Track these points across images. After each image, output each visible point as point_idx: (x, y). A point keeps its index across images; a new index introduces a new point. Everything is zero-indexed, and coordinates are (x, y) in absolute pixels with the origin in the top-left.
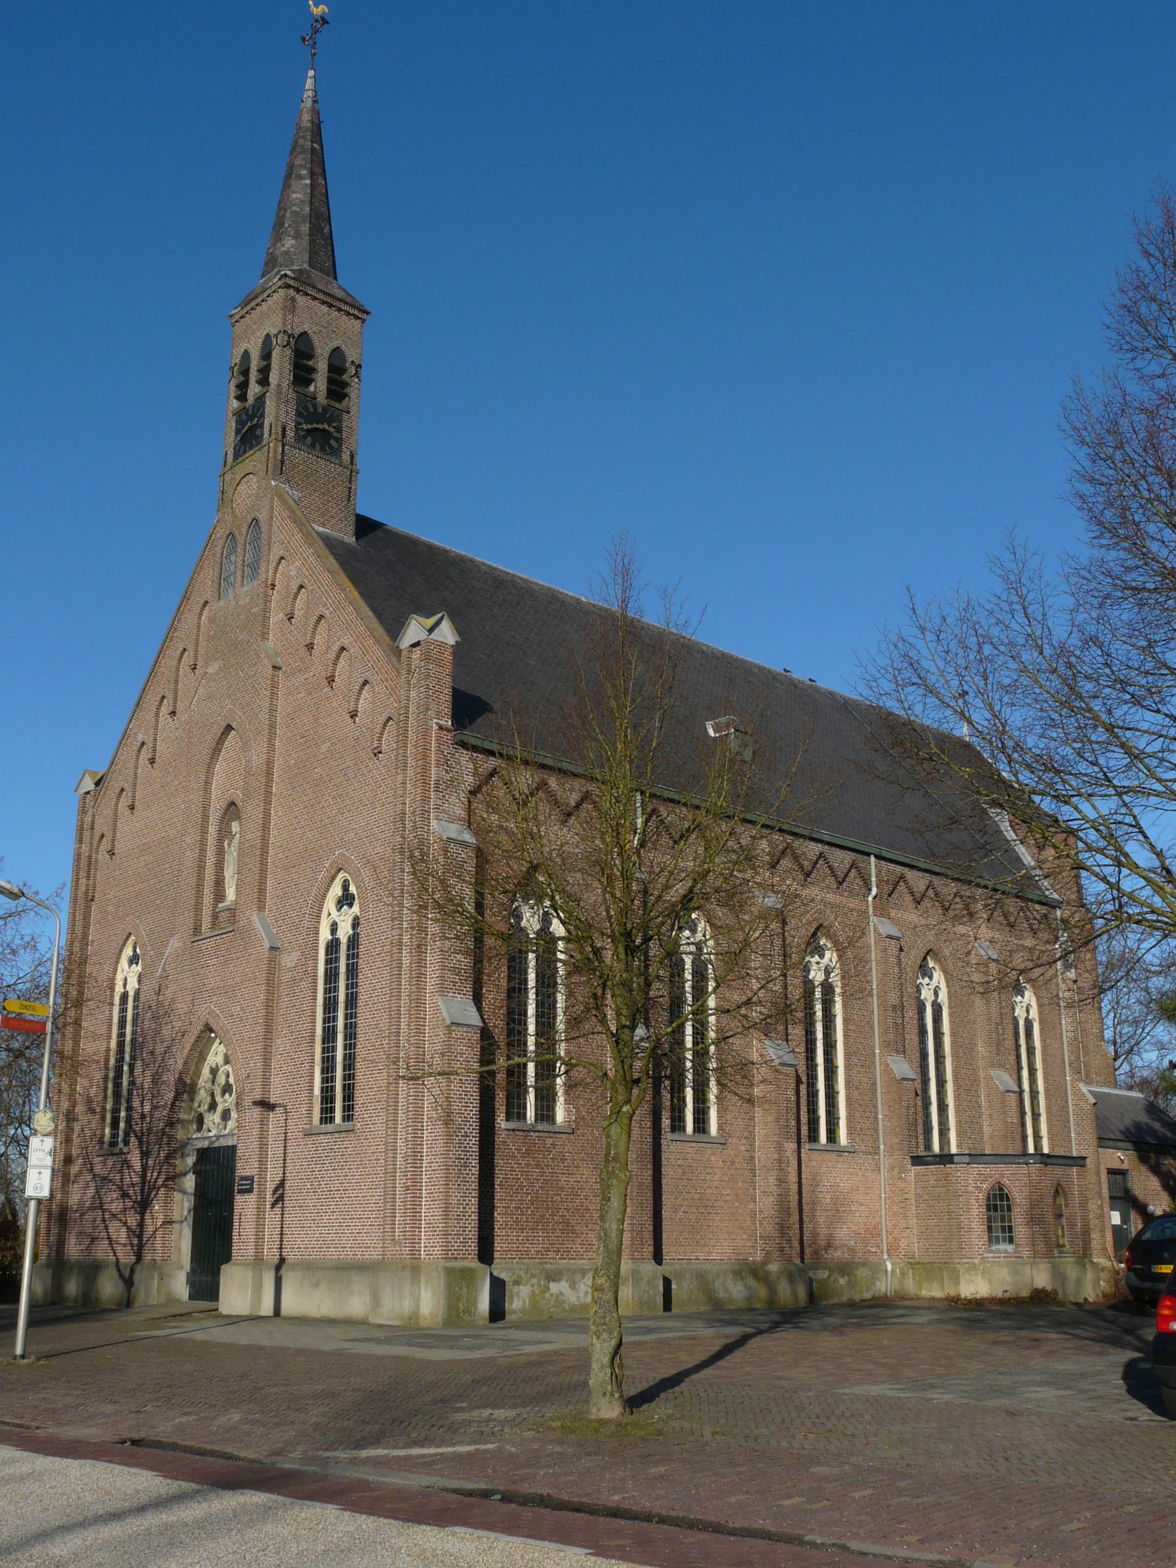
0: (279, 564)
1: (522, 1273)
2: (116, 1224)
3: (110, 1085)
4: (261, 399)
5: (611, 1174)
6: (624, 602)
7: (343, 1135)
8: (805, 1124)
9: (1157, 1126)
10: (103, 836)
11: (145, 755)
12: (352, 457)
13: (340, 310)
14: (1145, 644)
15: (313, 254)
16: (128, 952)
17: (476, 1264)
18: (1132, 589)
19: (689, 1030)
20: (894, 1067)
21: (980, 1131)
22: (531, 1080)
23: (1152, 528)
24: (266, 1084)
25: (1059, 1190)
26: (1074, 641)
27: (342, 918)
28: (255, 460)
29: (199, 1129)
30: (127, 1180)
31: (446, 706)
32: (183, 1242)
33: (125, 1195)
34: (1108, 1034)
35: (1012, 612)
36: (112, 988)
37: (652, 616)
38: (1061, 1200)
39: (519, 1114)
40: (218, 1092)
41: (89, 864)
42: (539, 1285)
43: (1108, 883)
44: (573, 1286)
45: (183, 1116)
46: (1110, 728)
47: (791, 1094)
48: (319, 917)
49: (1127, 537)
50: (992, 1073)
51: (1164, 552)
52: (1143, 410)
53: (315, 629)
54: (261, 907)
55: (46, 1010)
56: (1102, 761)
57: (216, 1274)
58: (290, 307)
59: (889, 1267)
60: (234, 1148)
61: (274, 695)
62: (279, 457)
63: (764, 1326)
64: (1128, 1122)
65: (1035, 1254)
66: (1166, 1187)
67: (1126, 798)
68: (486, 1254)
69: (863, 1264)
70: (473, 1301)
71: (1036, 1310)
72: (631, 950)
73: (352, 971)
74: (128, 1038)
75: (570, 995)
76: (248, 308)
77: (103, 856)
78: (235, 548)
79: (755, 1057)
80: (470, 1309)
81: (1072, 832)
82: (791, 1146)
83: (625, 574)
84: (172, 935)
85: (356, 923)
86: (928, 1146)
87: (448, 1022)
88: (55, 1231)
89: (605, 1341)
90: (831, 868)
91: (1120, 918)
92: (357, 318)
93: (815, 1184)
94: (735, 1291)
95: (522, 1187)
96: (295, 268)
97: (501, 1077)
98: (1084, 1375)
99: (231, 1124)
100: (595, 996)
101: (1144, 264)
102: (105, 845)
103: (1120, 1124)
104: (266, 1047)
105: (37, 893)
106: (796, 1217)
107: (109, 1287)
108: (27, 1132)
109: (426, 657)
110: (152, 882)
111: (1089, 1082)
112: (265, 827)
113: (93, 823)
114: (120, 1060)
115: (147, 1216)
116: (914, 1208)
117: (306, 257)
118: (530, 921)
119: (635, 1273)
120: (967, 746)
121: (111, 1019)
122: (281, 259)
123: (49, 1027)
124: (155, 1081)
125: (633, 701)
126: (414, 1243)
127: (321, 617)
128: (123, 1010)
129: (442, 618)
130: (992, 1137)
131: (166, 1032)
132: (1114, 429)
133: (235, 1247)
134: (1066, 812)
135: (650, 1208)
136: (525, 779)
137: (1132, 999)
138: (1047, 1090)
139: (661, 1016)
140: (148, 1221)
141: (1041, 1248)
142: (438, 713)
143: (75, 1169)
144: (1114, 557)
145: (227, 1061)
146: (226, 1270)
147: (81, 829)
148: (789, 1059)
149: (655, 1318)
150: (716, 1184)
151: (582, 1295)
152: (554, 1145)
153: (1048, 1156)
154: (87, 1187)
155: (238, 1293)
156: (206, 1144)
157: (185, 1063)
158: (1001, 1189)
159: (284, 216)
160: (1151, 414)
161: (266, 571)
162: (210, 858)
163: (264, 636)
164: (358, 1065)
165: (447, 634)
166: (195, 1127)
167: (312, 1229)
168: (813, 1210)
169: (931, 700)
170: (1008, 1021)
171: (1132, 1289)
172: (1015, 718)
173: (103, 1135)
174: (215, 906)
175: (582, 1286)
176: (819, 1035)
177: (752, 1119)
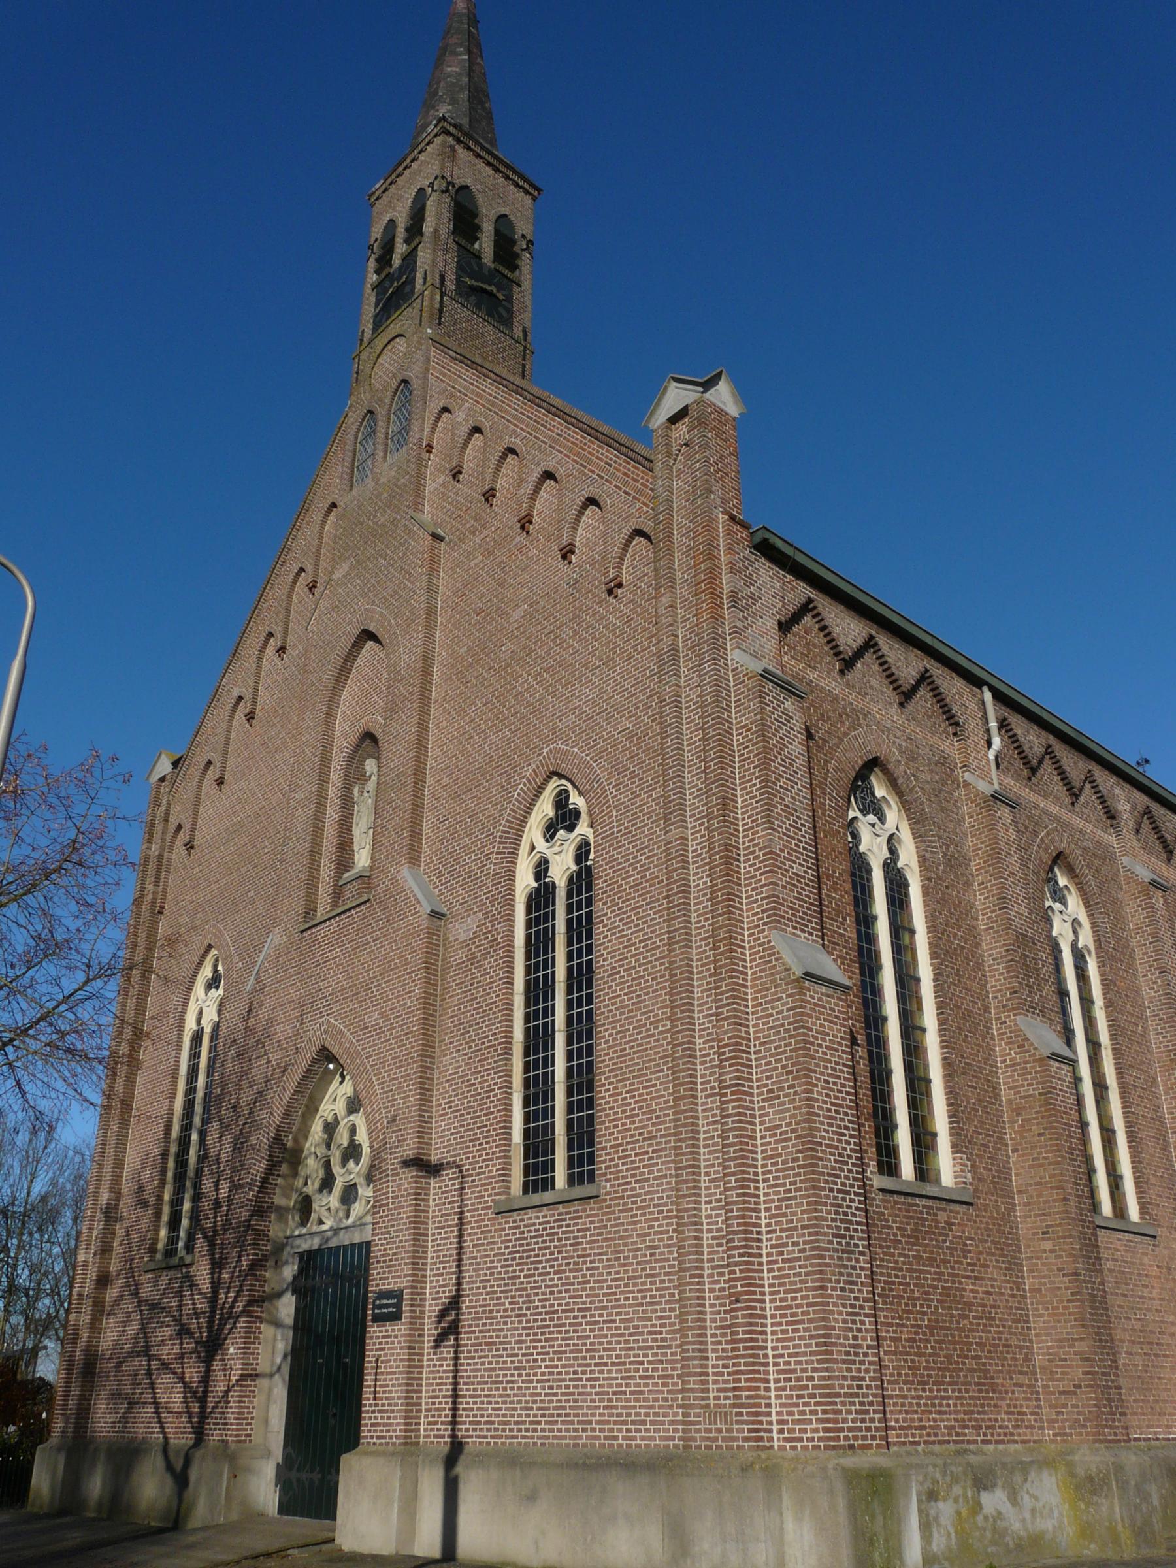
0: (438, 419)
1: (938, 1475)
3: (171, 1164)
7: (576, 1206)
10: (179, 827)
13: (507, 178)
24: (423, 1132)
27: (556, 849)
28: (405, 320)
29: (304, 1222)
30: (188, 1308)
32: (267, 1414)
33: (183, 1331)
40: (336, 1158)
41: (159, 867)
44: (1014, 1498)
45: (278, 1200)
48: (514, 854)
54: (414, 860)
57: (331, 1468)
62: (437, 306)
74: (200, 1094)
85: (582, 853)
87: (799, 973)
99: (357, 1209)
102: (183, 837)
110: (244, 870)
112: (421, 744)
113: (167, 814)
114: (186, 1128)
115: (217, 1365)
121: (176, 1069)
128: (195, 1056)
131: (258, 1071)
143: (112, 1293)
151: (1028, 1516)
154: (127, 1321)
155: (374, 1509)
156: (315, 1243)
157: (286, 1114)
161: (419, 431)
162: (332, 814)
163: (418, 506)
164: (600, 1080)
166: (297, 1218)
173: (155, 1241)
175: (1026, 1497)
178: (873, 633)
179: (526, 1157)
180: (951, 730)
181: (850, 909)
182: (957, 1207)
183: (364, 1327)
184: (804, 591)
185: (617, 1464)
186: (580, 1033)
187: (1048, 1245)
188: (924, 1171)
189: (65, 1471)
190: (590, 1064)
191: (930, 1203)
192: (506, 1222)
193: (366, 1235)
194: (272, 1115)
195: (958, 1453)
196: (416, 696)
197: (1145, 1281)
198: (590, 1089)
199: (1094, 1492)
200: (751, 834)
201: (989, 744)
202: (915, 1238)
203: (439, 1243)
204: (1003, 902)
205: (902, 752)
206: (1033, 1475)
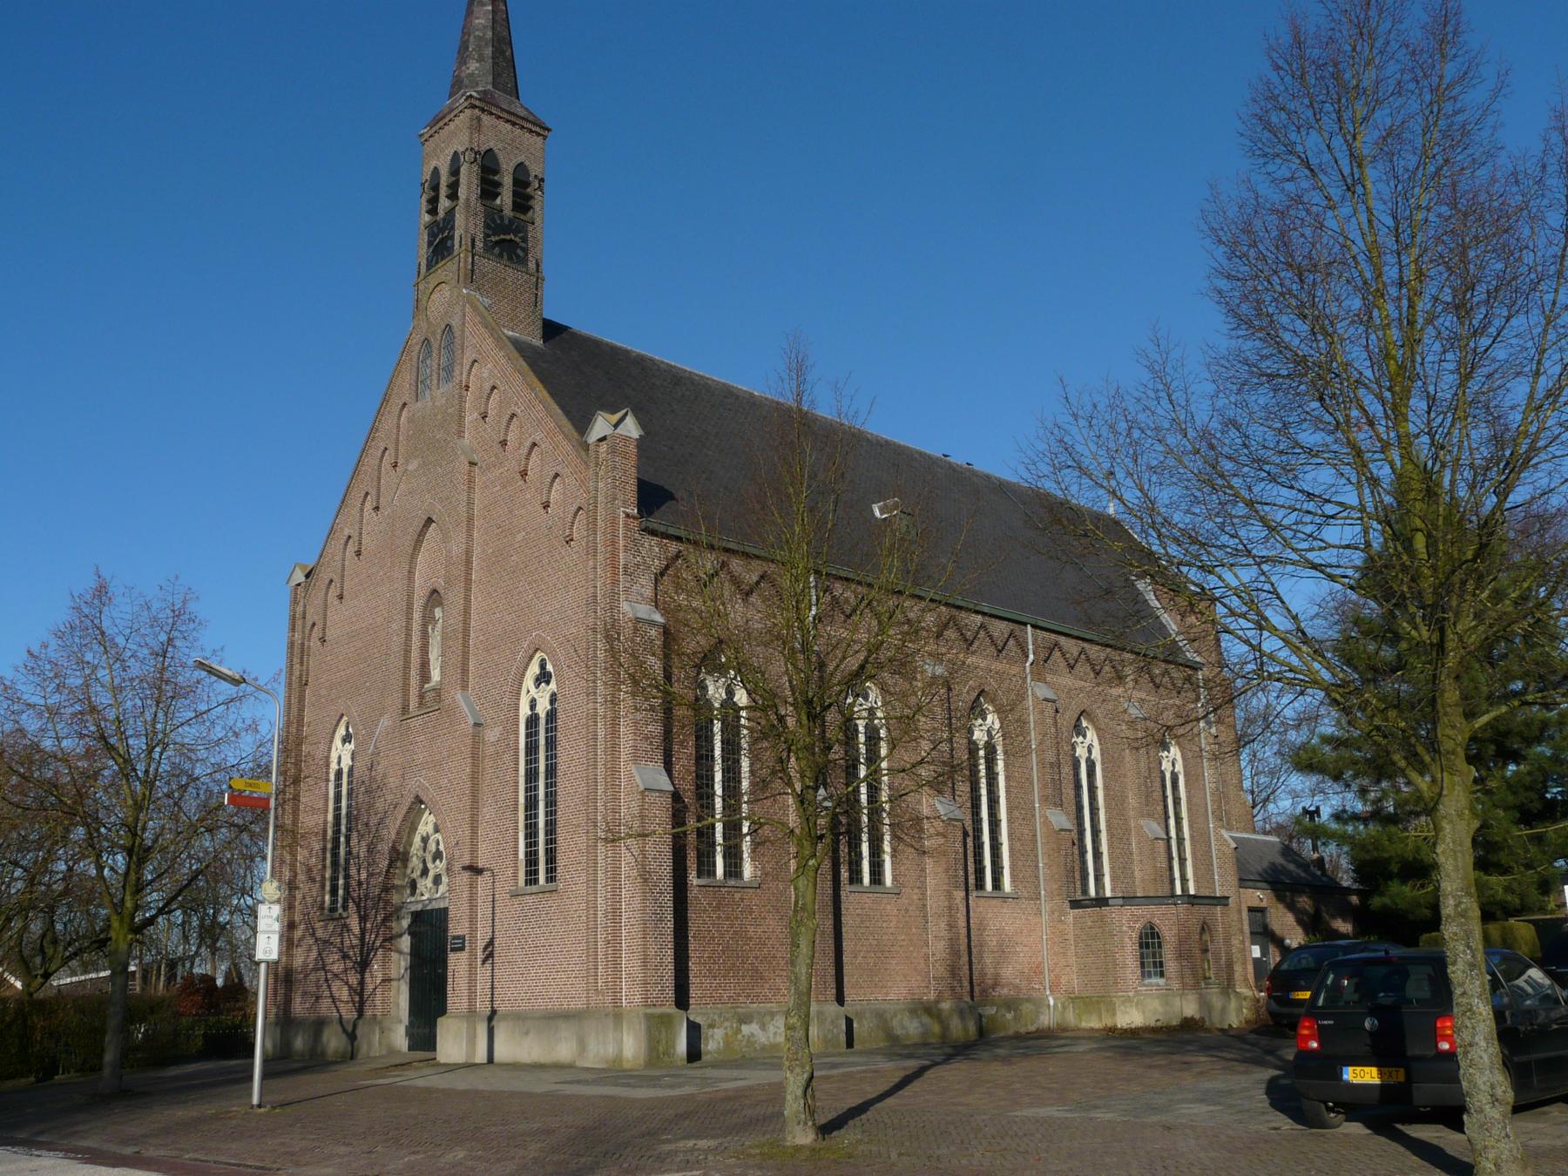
2: (338, 983)
3: (328, 855)
4: (451, 213)
5: (800, 923)
6: (799, 395)
8: (972, 876)
9: (1292, 867)
11: (352, 548)
12: (538, 265)
13: (522, 127)
14: (1279, 425)
16: (341, 731)
17: (673, 1010)
18: (1268, 375)
19: (863, 790)
20: (1052, 819)
21: (1132, 876)
22: (719, 838)
23: (1284, 319)
24: (474, 851)
25: (1205, 928)
26: (1215, 425)
28: (447, 270)
29: (413, 893)
32: (401, 998)
33: (345, 957)
34: (1247, 784)
35: (1158, 399)
36: (328, 766)
37: (824, 408)
38: (1206, 937)
40: (429, 859)
43: (1251, 645)
44: (763, 1027)
45: (396, 882)
46: (1250, 504)
47: (959, 846)
48: (519, 694)
49: (1261, 329)
50: (1142, 822)
51: (1296, 341)
52: (1273, 211)
53: (508, 426)
54: (465, 687)
55: (269, 787)
56: (1242, 533)
57: (433, 1026)
58: (477, 126)
60: (446, 910)
61: (471, 489)
63: (938, 1059)
64: (1265, 864)
65: (1184, 986)
66: (1300, 922)
67: (1265, 567)
68: (682, 1001)
69: (1028, 1000)
70: (671, 1044)
71: (1186, 1036)
72: (812, 717)
73: (551, 743)
74: (344, 812)
75: (755, 759)
77: (314, 643)
78: (430, 353)
79: (926, 811)
81: (1214, 600)
82: (960, 894)
83: (799, 370)
84: (381, 715)
86: (1085, 891)
87: (642, 788)
88: (281, 991)
90: (991, 637)
91: (1262, 676)
92: (539, 134)
93: (982, 928)
94: (911, 1028)
95: (713, 938)
97: (692, 838)
98: (1231, 1092)
99: (442, 888)
100: (781, 761)
101: (1274, 77)
103: (1259, 866)
104: (473, 816)
105: (256, 679)
106: (965, 959)
107: (333, 1041)
108: (250, 901)
109: (613, 451)
111: (1230, 829)
112: (467, 612)
114: (337, 832)
115: (367, 975)
118: (715, 691)
119: (820, 1013)
120: (1117, 523)
122: (466, 81)
123: (272, 803)
124: (370, 851)
125: (809, 486)
127: (513, 415)
128: (338, 786)
130: (1143, 881)
131: (380, 805)
132: (1248, 230)
134: (1212, 581)
135: (832, 955)
136: (709, 561)
137: (1268, 753)
138: (1192, 837)
139: (837, 779)
140: (368, 979)
141: (1189, 980)
142: (624, 502)
143: (298, 933)
144: (1250, 347)
145: (437, 830)
146: (441, 1021)
147: (293, 619)
148: (958, 814)
149: (840, 1054)
152: (742, 899)
153: (1195, 897)
154: (310, 950)
155: (453, 1043)
156: (419, 907)
160: (1282, 214)
161: (460, 374)
163: (460, 434)
164: (559, 830)
165: (631, 428)
167: (518, 984)
168: (981, 953)
169: (1086, 481)
170: (1156, 774)
171: (1271, 1013)
172: (1164, 496)
176: (984, 792)
177: (923, 870)
188: (733, 869)
189: (237, 1058)
192: (516, 901)
194: (390, 832)
202: (718, 907)
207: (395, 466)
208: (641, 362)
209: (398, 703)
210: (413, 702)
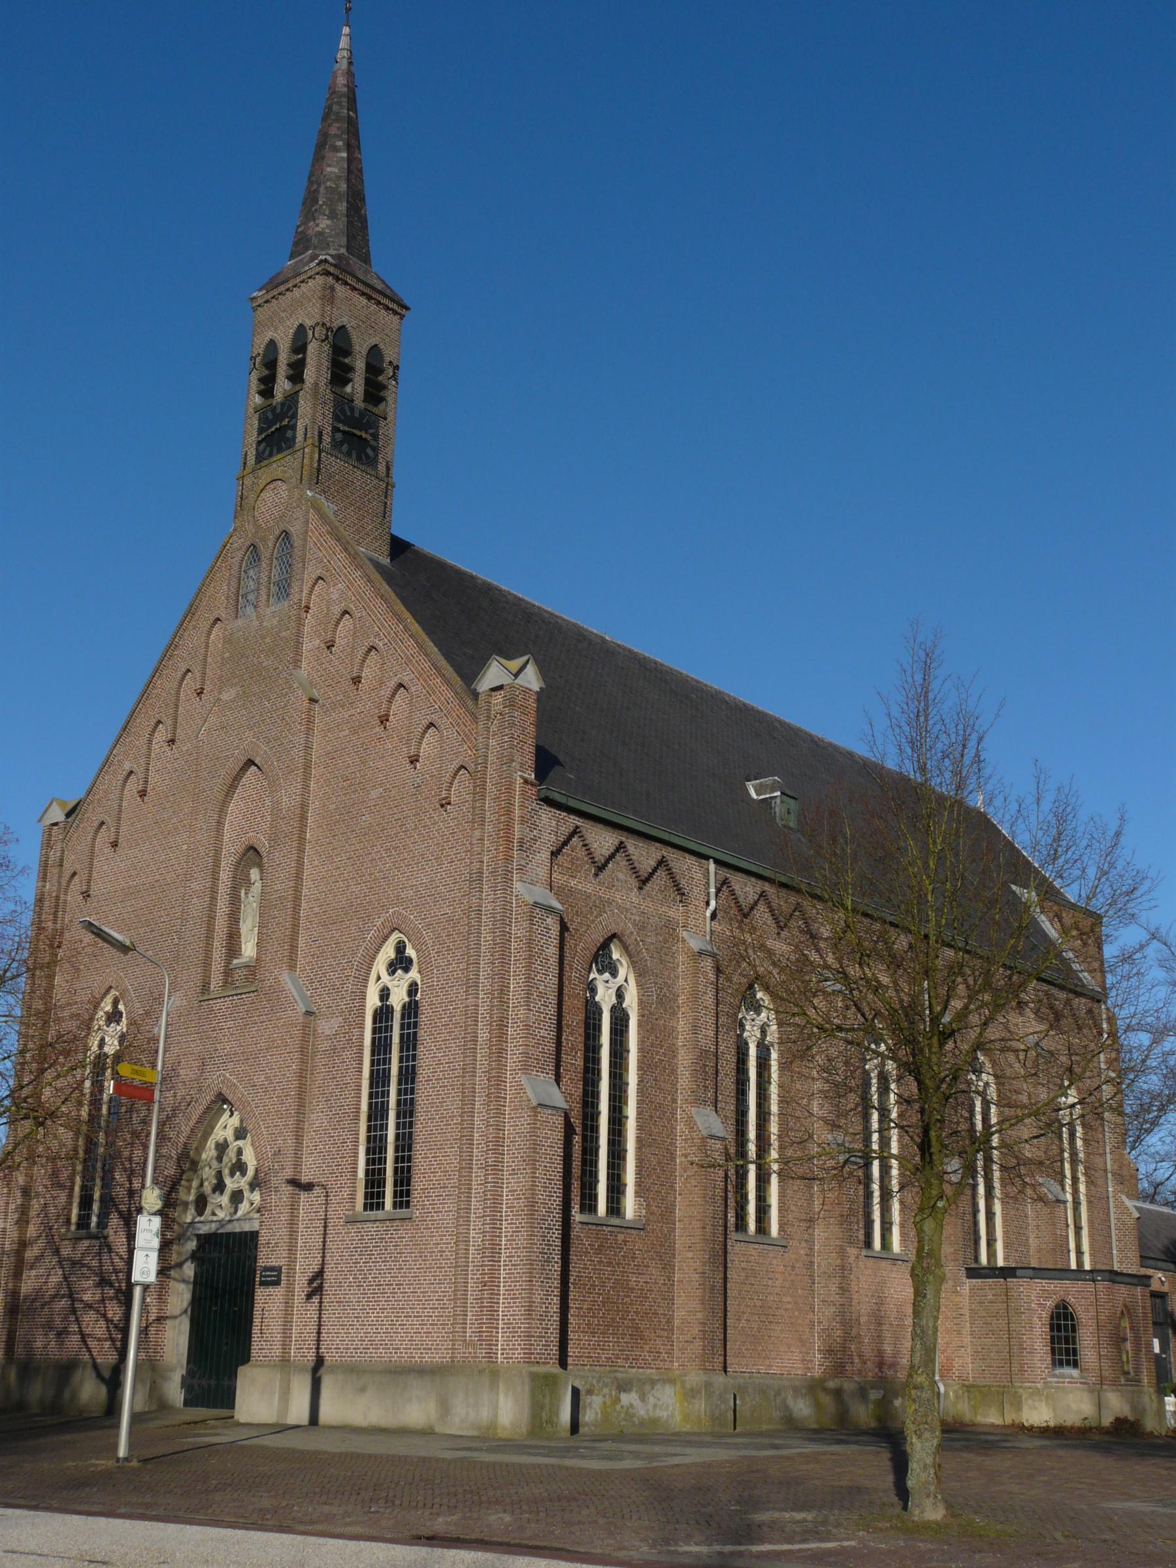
4: (291, 401)
7: (397, 1223)
11: (133, 786)
12: (388, 469)
13: (379, 303)
15: (351, 238)
17: (557, 1370)
21: (1026, 1244)
24: (297, 1165)
27: (396, 983)
28: (284, 465)
31: (530, 760)
39: (590, 1205)
40: (226, 1172)
42: (611, 1395)
44: (643, 1398)
48: (366, 980)
54: (292, 967)
58: (329, 297)
59: (942, 1389)
60: (254, 1235)
61: (309, 730)
70: (555, 1412)
76: (275, 292)
80: (552, 1421)
85: (413, 989)
86: (976, 1259)
87: (535, 1104)
89: (927, 1440)
92: (395, 313)
95: (593, 1286)
96: (332, 252)
99: (244, 1207)
102: (77, 885)
109: (511, 703)
112: (299, 877)
113: (62, 860)
116: (968, 1324)
117: (344, 241)
122: (315, 241)
126: (491, 1345)
129: (527, 662)
130: (1039, 1250)
133: (255, 1346)
146: (243, 1371)
150: (778, 1290)
151: (651, 1408)
152: (625, 1241)
158: (1065, 1308)
159: (317, 191)
161: (301, 591)
162: (222, 907)
163: (296, 663)
165: (532, 679)
167: (356, 1327)
174: (228, 962)
175: (651, 1398)
178: (624, 839)
179: (366, 1187)
180: (678, 898)
181: (581, 1046)
182: (633, 1231)
183: (254, 1289)
184: (574, 821)
185: (413, 1371)
186: (405, 1112)
187: (690, 1255)
188: (615, 1207)
190: (411, 1133)
191: (613, 1229)
192: (353, 1229)
193: (255, 1226)
195: (610, 1372)
196: (295, 837)
197: (771, 1275)
198: (410, 1150)
199: (693, 1397)
200: (517, 1013)
201: (708, 904)
202: (599, 1251)
203: (308, 1237)
204: (695, 1029)
205: (635, 924)
206: (658, 1386)
207: (200, 693)
208: (488, 591)
209: (198, 980)
210: (216, 981)
